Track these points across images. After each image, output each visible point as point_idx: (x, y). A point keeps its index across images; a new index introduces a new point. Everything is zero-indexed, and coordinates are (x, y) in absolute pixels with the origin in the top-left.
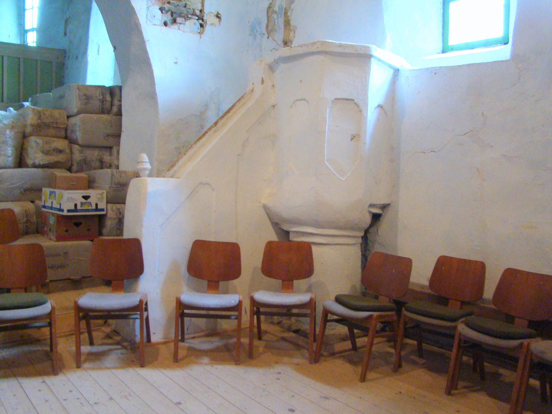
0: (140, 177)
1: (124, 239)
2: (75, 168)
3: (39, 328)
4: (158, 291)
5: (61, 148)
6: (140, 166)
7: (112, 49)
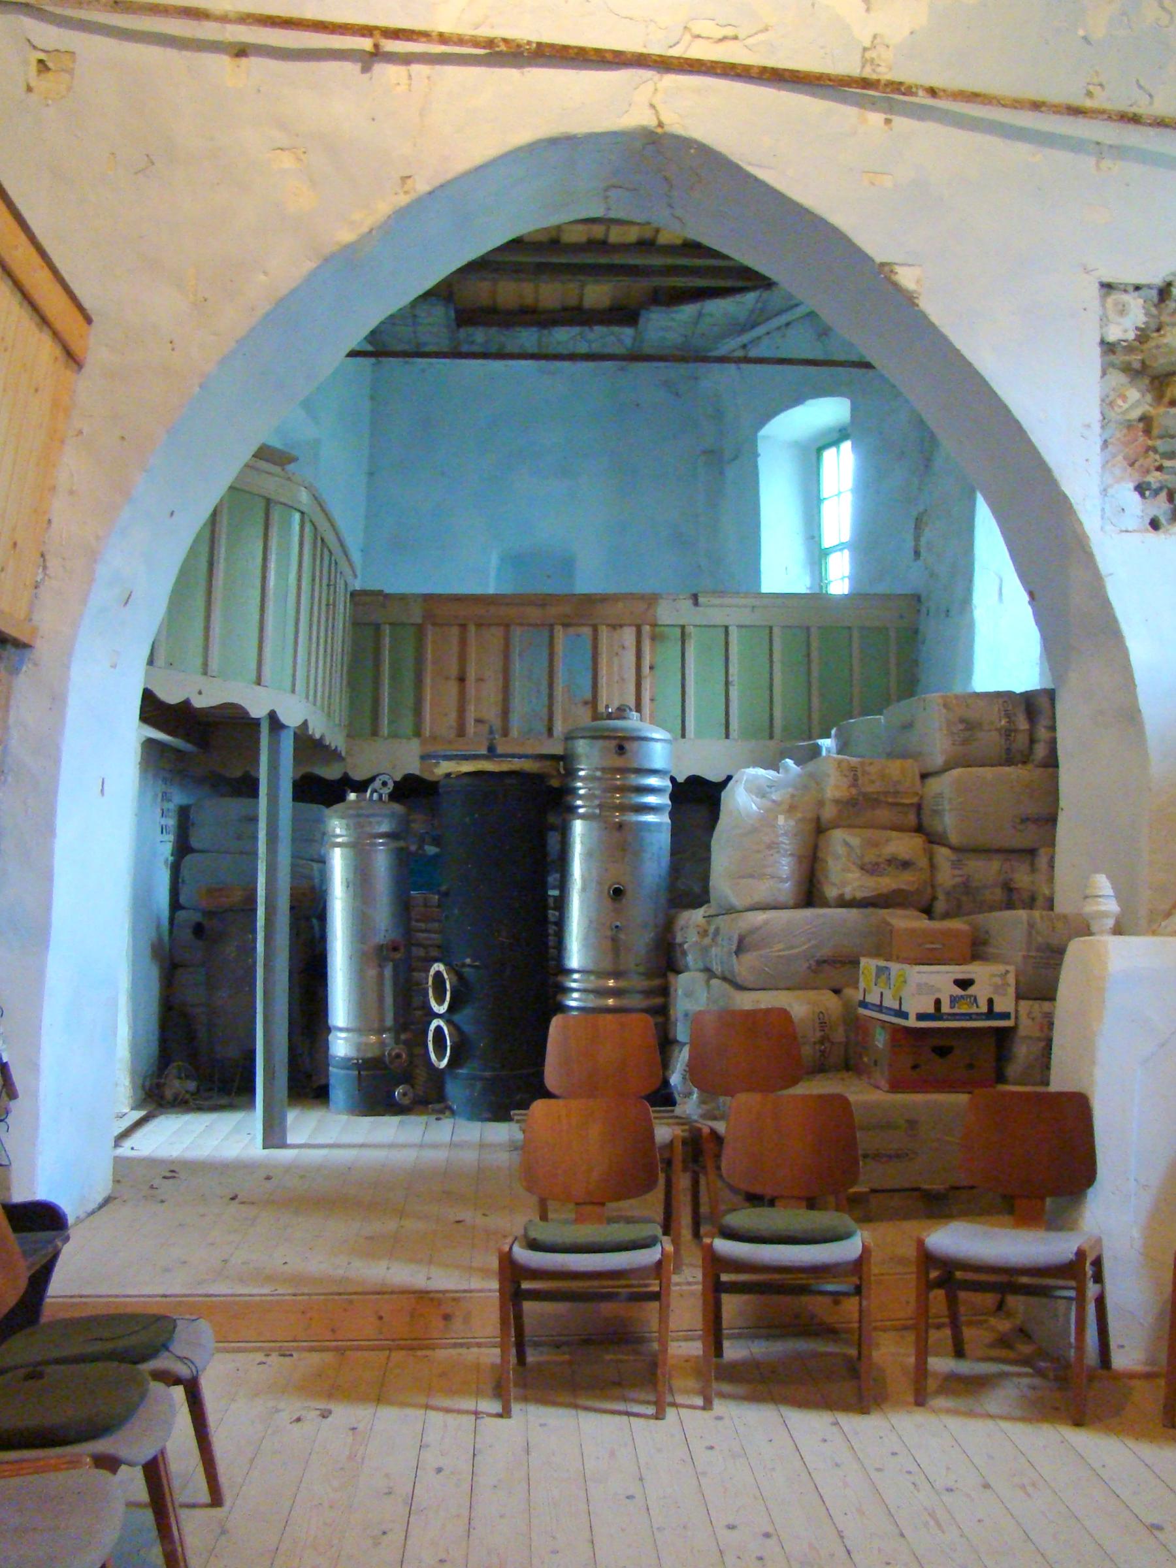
0: (1090, 934)
1: (1049, 1093)
2: (940, 906)
3: (837, 1297)
4: (1136, 1233)
5: (907, 857)
6: (1090, 908)
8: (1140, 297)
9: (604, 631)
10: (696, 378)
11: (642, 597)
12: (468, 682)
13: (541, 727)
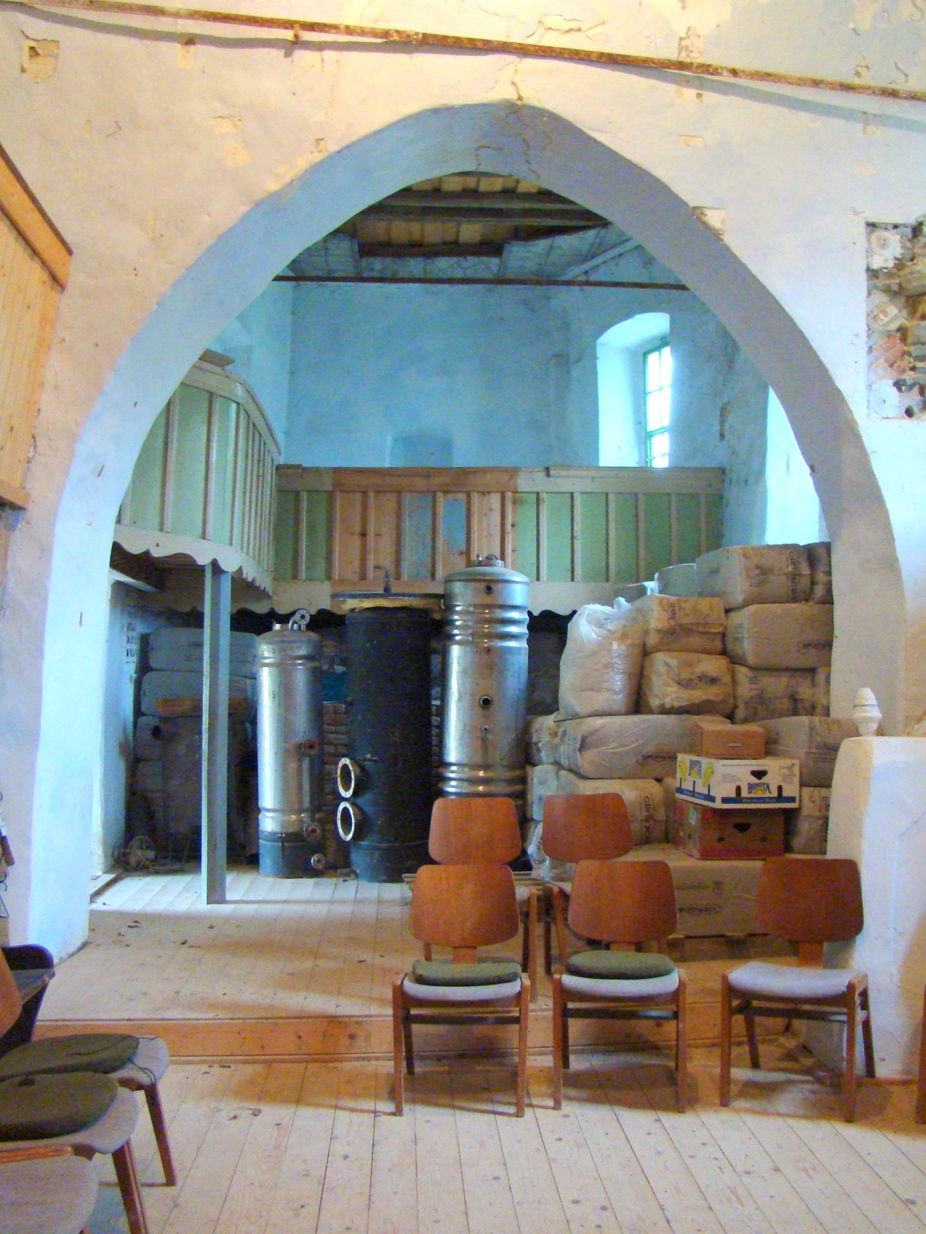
0: (859, 735)
1: (825, 860)
2: (740, 713)
3: (659, 1020)
4: (894, 970)
5: (714, 675)
6: (858, 715)
7: (808, 471)
8: (898, 234)
9: (475, 496)
10: (548, 298)
11: (506, 470)
12: (368, 537)
13: (426, 572)
